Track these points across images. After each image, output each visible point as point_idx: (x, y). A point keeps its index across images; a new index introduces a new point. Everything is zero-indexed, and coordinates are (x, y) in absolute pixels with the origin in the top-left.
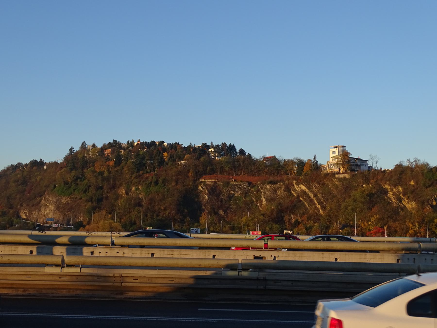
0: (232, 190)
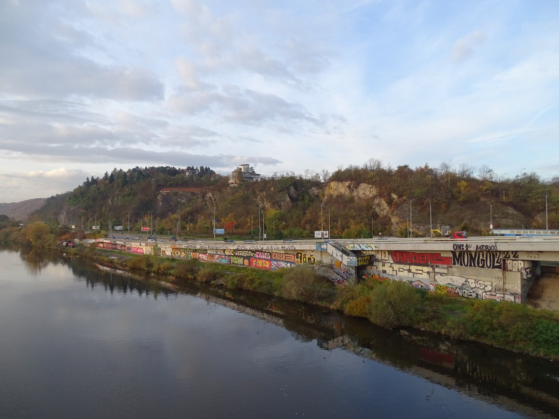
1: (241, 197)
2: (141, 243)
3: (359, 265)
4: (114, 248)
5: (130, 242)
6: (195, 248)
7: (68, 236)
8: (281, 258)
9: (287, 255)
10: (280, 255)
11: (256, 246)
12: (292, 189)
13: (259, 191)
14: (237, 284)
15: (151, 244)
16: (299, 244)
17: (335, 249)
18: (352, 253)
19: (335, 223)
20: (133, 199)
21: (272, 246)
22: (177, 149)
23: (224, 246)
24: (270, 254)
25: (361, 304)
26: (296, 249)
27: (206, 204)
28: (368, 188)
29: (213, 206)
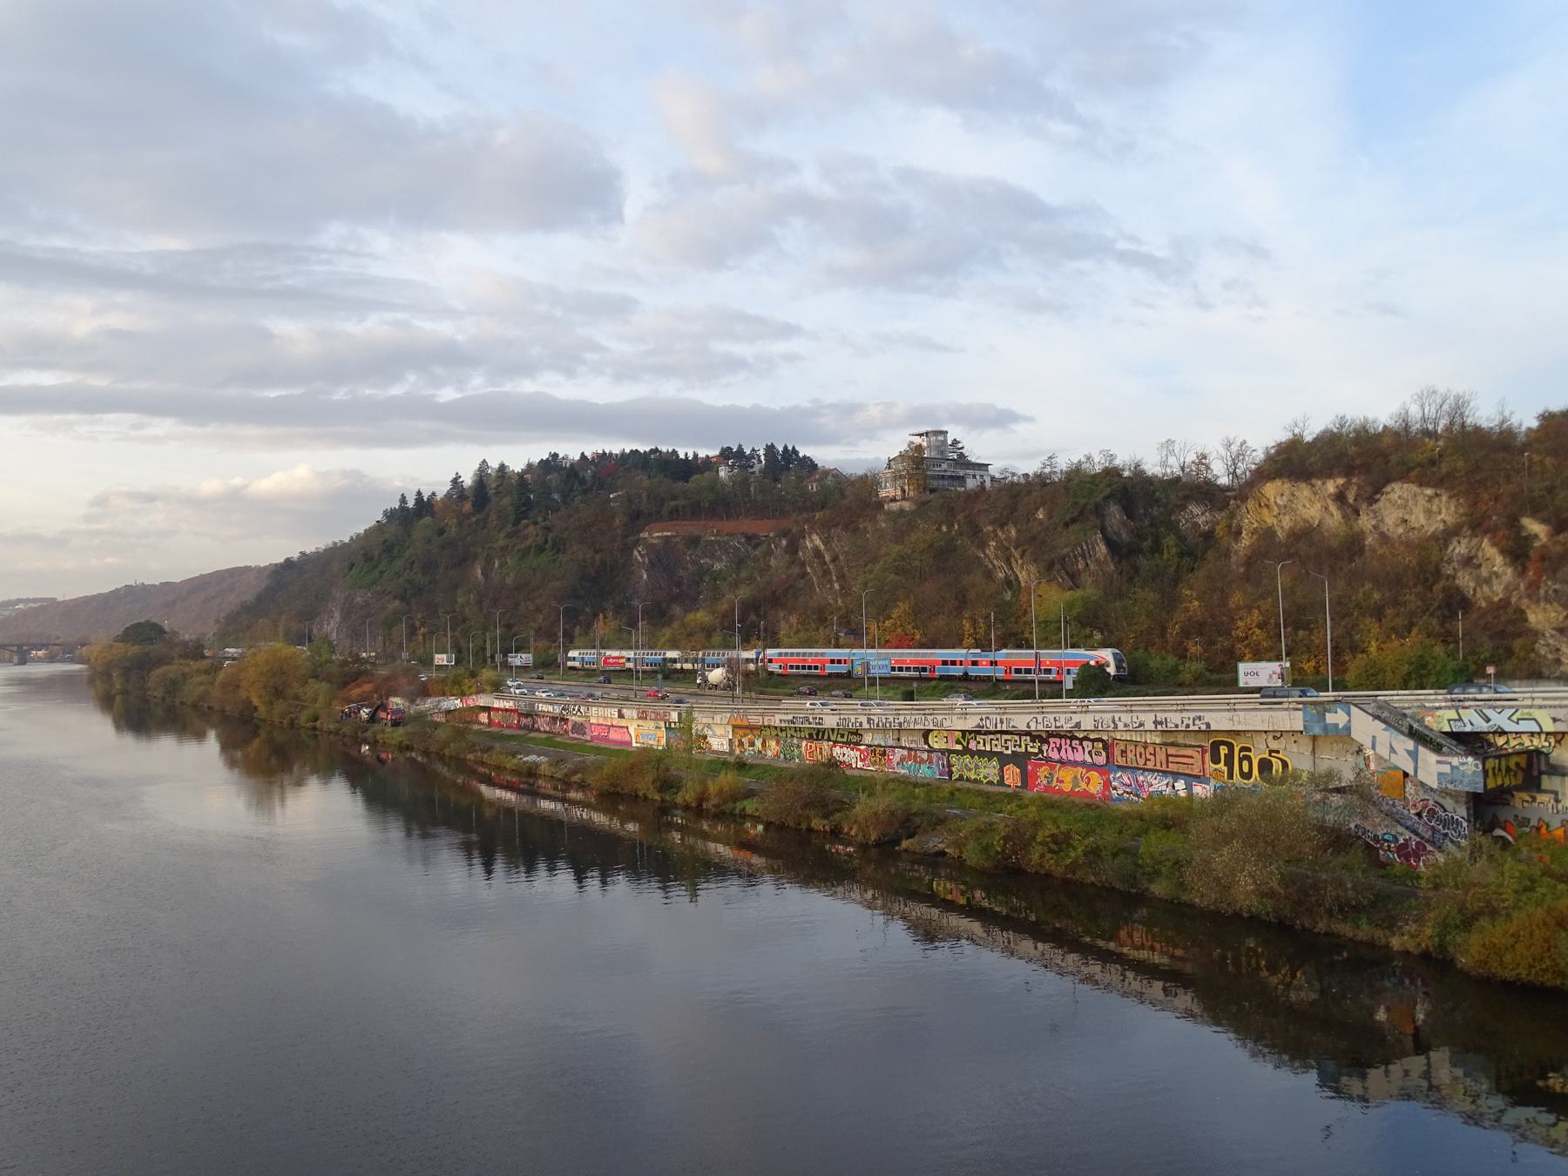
0: (706, 557)
1: (930, 546)
2: (624, 711)
3: (1489, 787)
4: (526, 727)
5: (583, 705)
6: (819, 724)
7: (367, 687)
8: (1147, 760)
9: (1171, 751)
10: (1145, 748)
11: (1051, 717)
12: (1115, 513)
13: (992, 523)
14: (1003, 851)
15: (658, 714)
16: (1225, 710)
17: (1384, 726)
18: (1454, 742)
19: (1301, 633)
20: (554, 560)
21: (1117, 719)
22: (670, 390)
23: (929, 717)
24: (1106, 746)
25: (1531, 935)
26: (1213, 728)
27: (804, 575)
28: (1422, 501)
29: (830, 582)
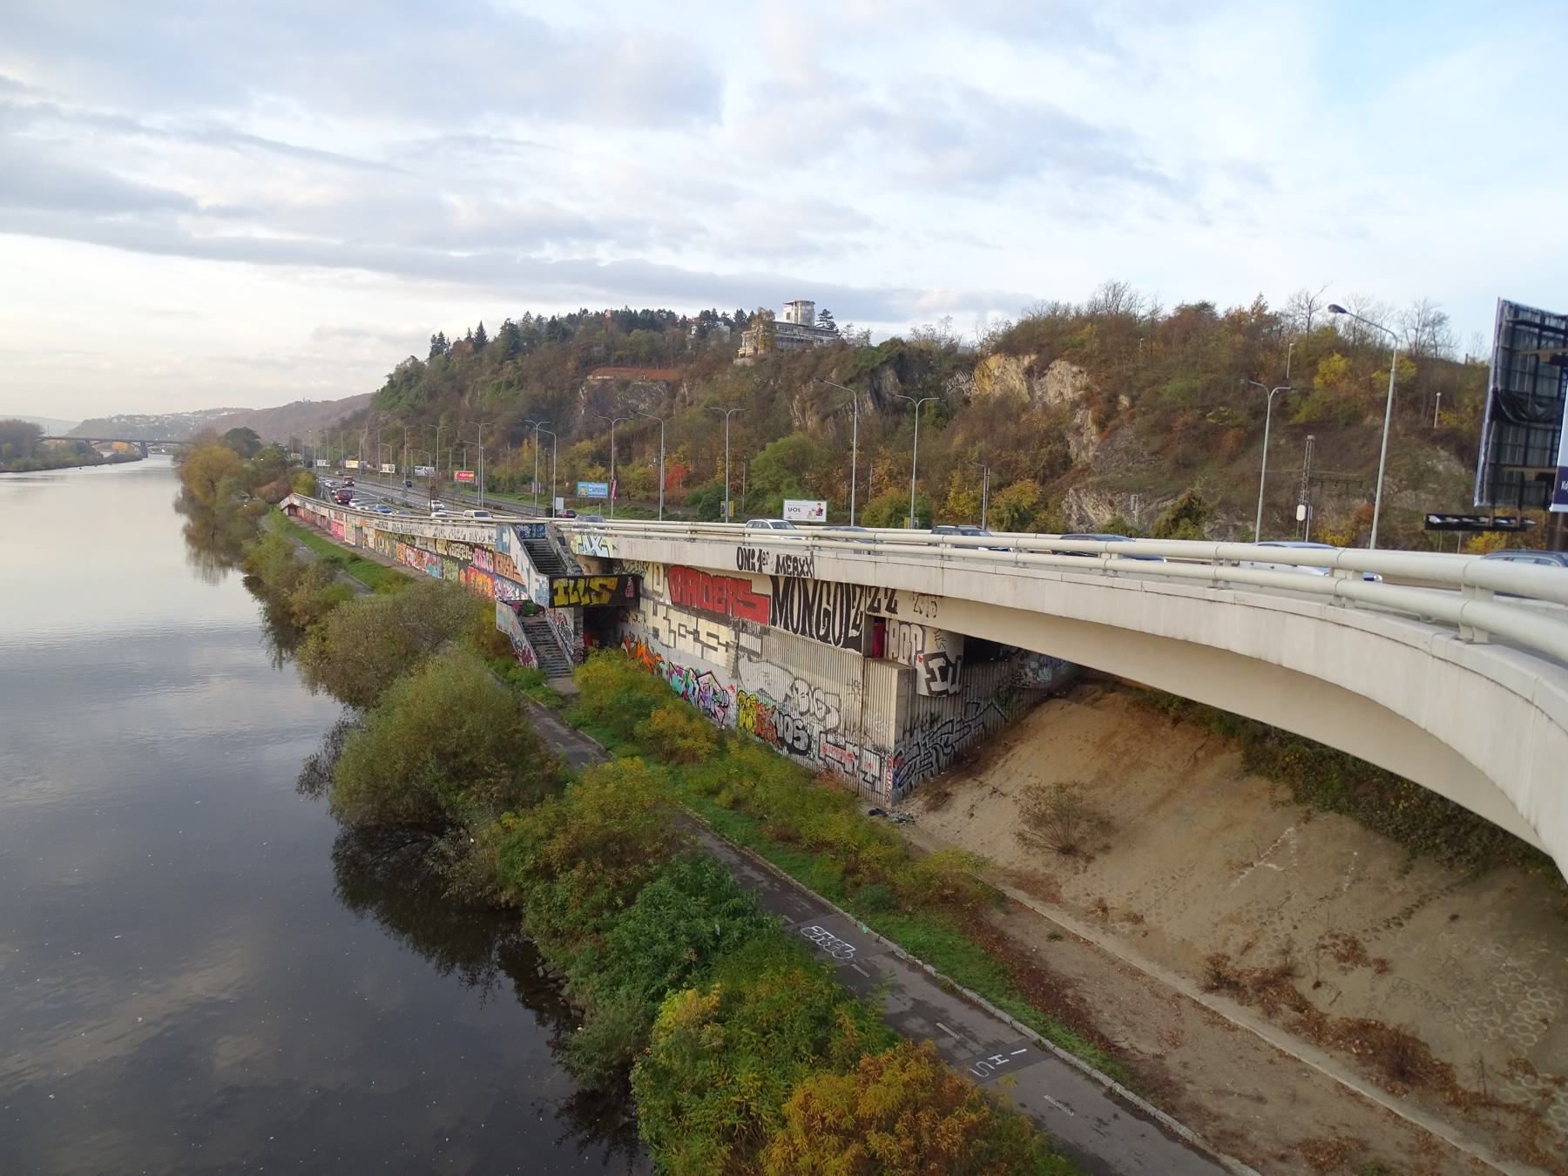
12: (889, 379)
